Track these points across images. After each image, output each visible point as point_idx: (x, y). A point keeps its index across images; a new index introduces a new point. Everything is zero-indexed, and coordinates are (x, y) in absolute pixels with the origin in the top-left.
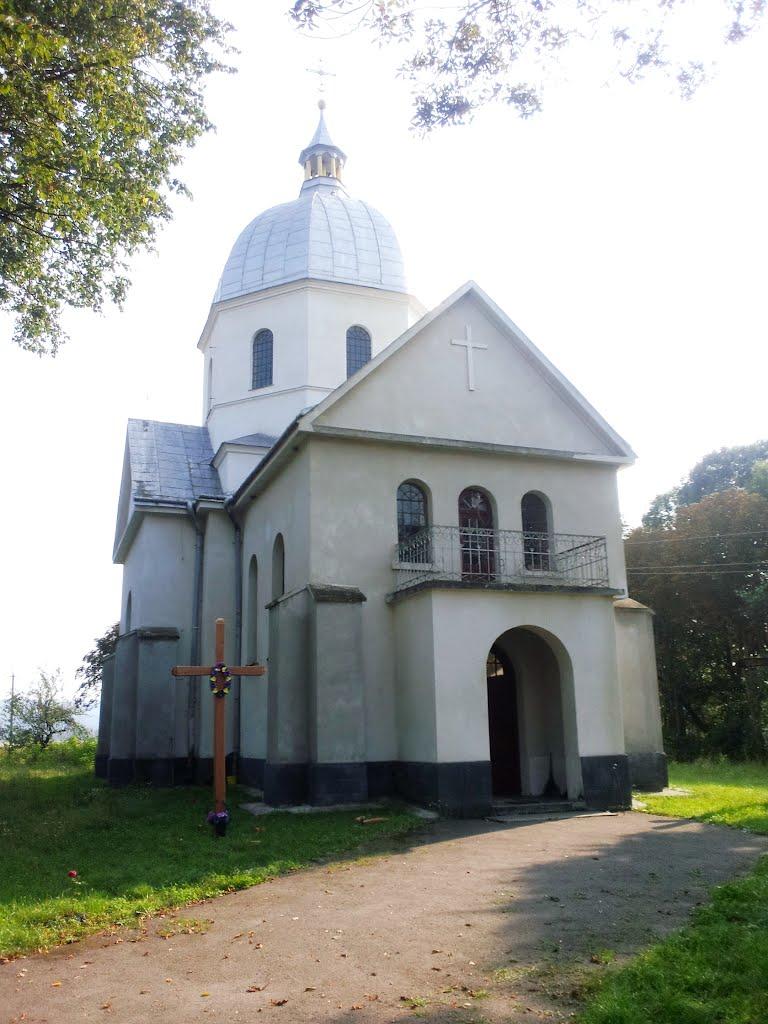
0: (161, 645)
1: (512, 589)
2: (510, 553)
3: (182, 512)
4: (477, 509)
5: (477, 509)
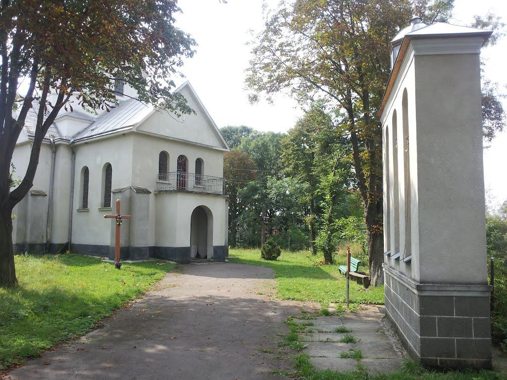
0: (39, 198)
1: (191, 192)
2: (191, 182)
3: (48, 143)
4: (182, 163)
5: (182, 163)
